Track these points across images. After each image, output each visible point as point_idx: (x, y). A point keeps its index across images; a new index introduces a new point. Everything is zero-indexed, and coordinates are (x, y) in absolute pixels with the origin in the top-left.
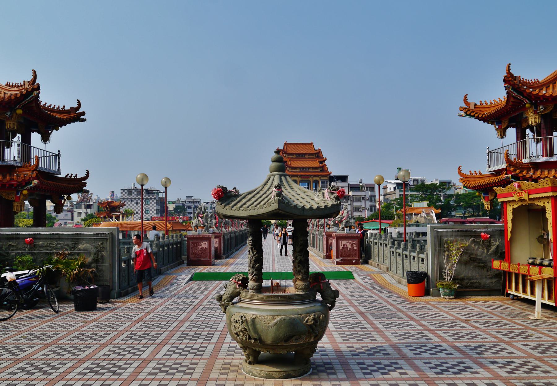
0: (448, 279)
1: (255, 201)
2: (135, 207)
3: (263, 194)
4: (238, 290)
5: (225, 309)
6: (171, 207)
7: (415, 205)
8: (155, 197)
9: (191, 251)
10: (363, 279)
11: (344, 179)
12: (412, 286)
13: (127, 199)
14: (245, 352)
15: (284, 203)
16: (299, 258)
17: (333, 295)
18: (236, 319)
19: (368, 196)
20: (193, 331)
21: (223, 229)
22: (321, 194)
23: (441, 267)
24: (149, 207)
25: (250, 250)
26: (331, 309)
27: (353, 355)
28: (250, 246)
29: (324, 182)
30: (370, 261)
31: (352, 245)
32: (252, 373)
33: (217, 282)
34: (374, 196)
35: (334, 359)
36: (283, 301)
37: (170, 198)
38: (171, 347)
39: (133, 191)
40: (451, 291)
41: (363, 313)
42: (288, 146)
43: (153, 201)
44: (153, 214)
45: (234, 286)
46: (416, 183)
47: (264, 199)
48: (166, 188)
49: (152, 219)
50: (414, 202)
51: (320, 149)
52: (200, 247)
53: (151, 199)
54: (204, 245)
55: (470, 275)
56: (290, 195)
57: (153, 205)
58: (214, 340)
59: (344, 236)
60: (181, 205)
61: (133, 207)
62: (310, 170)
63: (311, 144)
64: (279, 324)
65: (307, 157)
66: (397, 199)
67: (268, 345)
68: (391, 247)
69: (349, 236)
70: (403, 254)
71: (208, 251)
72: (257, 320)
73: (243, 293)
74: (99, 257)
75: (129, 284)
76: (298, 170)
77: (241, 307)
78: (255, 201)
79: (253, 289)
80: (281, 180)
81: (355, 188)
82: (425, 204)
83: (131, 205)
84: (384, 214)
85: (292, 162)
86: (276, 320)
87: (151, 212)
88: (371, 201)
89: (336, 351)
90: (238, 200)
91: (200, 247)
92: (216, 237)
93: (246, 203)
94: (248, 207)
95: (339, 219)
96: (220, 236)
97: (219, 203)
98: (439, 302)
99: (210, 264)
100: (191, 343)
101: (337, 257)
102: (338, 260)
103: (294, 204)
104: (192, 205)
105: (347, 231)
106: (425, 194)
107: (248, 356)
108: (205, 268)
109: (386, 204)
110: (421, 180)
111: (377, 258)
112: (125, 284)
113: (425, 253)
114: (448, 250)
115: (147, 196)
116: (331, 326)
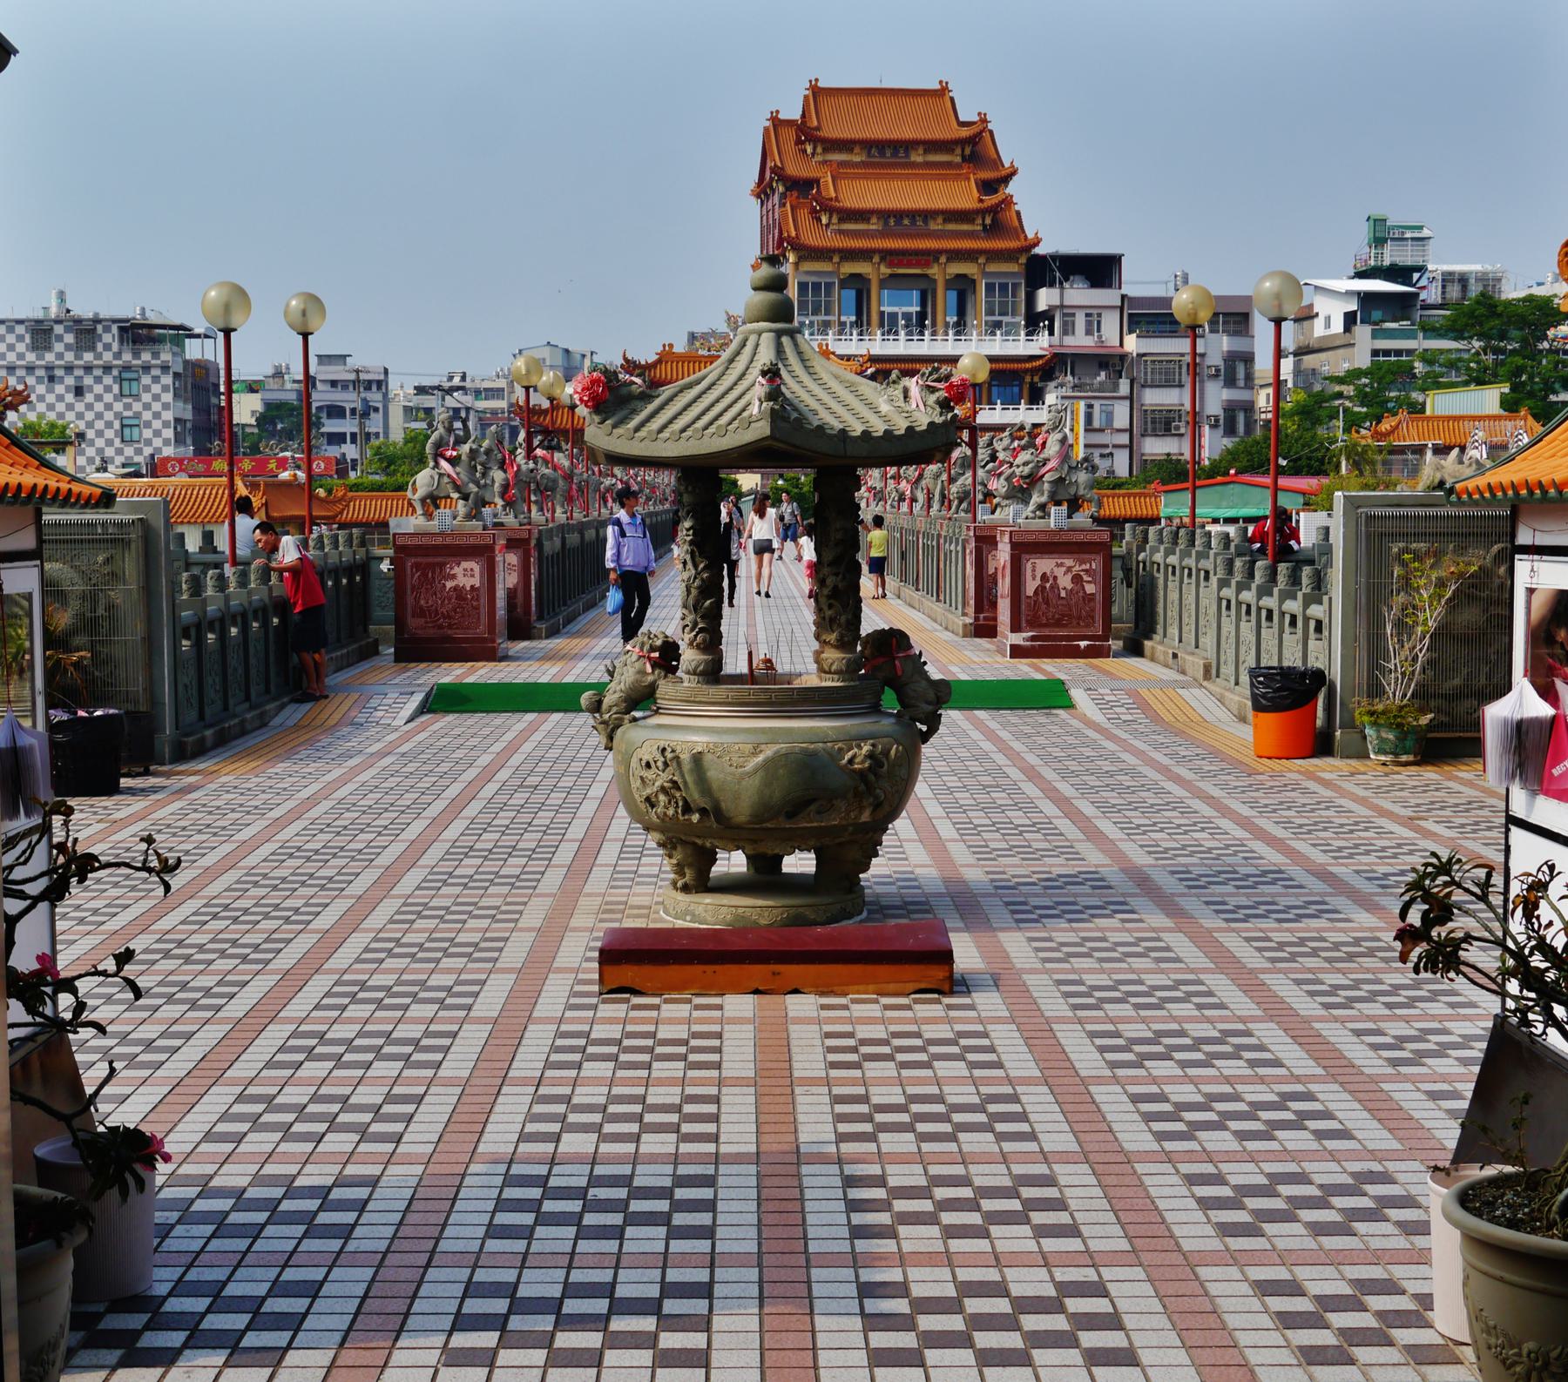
0: (1396, 692)
1: (703, 413)
2: (70, 407)
3: (727, 392)
4: (650, 678)
5: (611, 738)
6: (246, 410)
7: (1440, 403)
8: (166, 356)
9: (410, 600)
10: (1099, 702)
11: (1100, 270)
12: (1269, 718)
13: (30, 369)
14: (670, 857)
15: (786, 419)
16: (830, 581)
17: (931, 695)
18: (646, 757)
19: (1215, 359)
20: (351, 1021)
21: (534, 513)
22: (899, 393)
23: (1376, 652)
24: (137, 407)
25: (688, 557)
26: (925, 737)
27: (997, 888)
28: (686, 547)
29: (1004, 287)
30: (1147, 644)
31: (1077, 579)
32: (693, 915)
33: (530, 717)
34: (1248, 359)
35: (940, 895)
36: (782, 704)
37: (244, 369)
38: (240, 1098)
39: (59, 329)
40: (1402, 738)
41: (1067, 800)
42: (827, 105)
43: (156, 379)
44: (158, 442)
45: (638, 665)
46: (1454, 292)
47: (730, 406)
48: (305, 336)
49: (157, 468)
50: (1439, 386)
51: (984, 121)
52: (449, 584)
53: (146, 368)
54: (466, 574)
55: (1483, 681)
56: (805, 396)
57: (156, 398)
58: (458, 1065)
59: (1042, 538)
60: (291, 397)
61: (60, 407)
62: (933, 226)
63: (943, 91)
64: (770, 766)
65: (917, 157)
66: (1355, 374)
67: (739, 827)
68: (1223, 583)
69: (1064, 538)
70: (1259, 609)
71: (484, 600)
72: (708, 758)
73: (665, 688)
74: (101, 611)
75: (201, 716)
76: (874, 225)
77: (660, 726)
78: (703, 413)
79: (694, 673)
80: (779, 350)
81: (1150, 317)
82: (1488, 399)
83: (50, 398)
84: (1290, 446)
85: (843, 184)
86: (761, 758)
87: (147, 433)
88: (1230, 382)
89: (946, 881)
90: (651, 407)
91: (449, 584)
92: (512, 544)
93: (675, 417)
94: (683, 430)
95: (1027, 470)
96: (527, 541)
97: (597, 419)
98: (1352, 774)
99: (492, 655)
100: (342, 1082)
101: (1015, 628)
102: (1018, 639)
103: (816, 423)
104: (349, 399)
105: (1057, 517)
106: (1497, 351)
107: (680, 869)
108: (472, 671)
109: (1302, 396)
110: (1482, 278)
111: (1173, 631)
112: (191, 715)
113: (1325, 598)
114: (1406, 585)
115: (127, 357)
116: (921, 789)
